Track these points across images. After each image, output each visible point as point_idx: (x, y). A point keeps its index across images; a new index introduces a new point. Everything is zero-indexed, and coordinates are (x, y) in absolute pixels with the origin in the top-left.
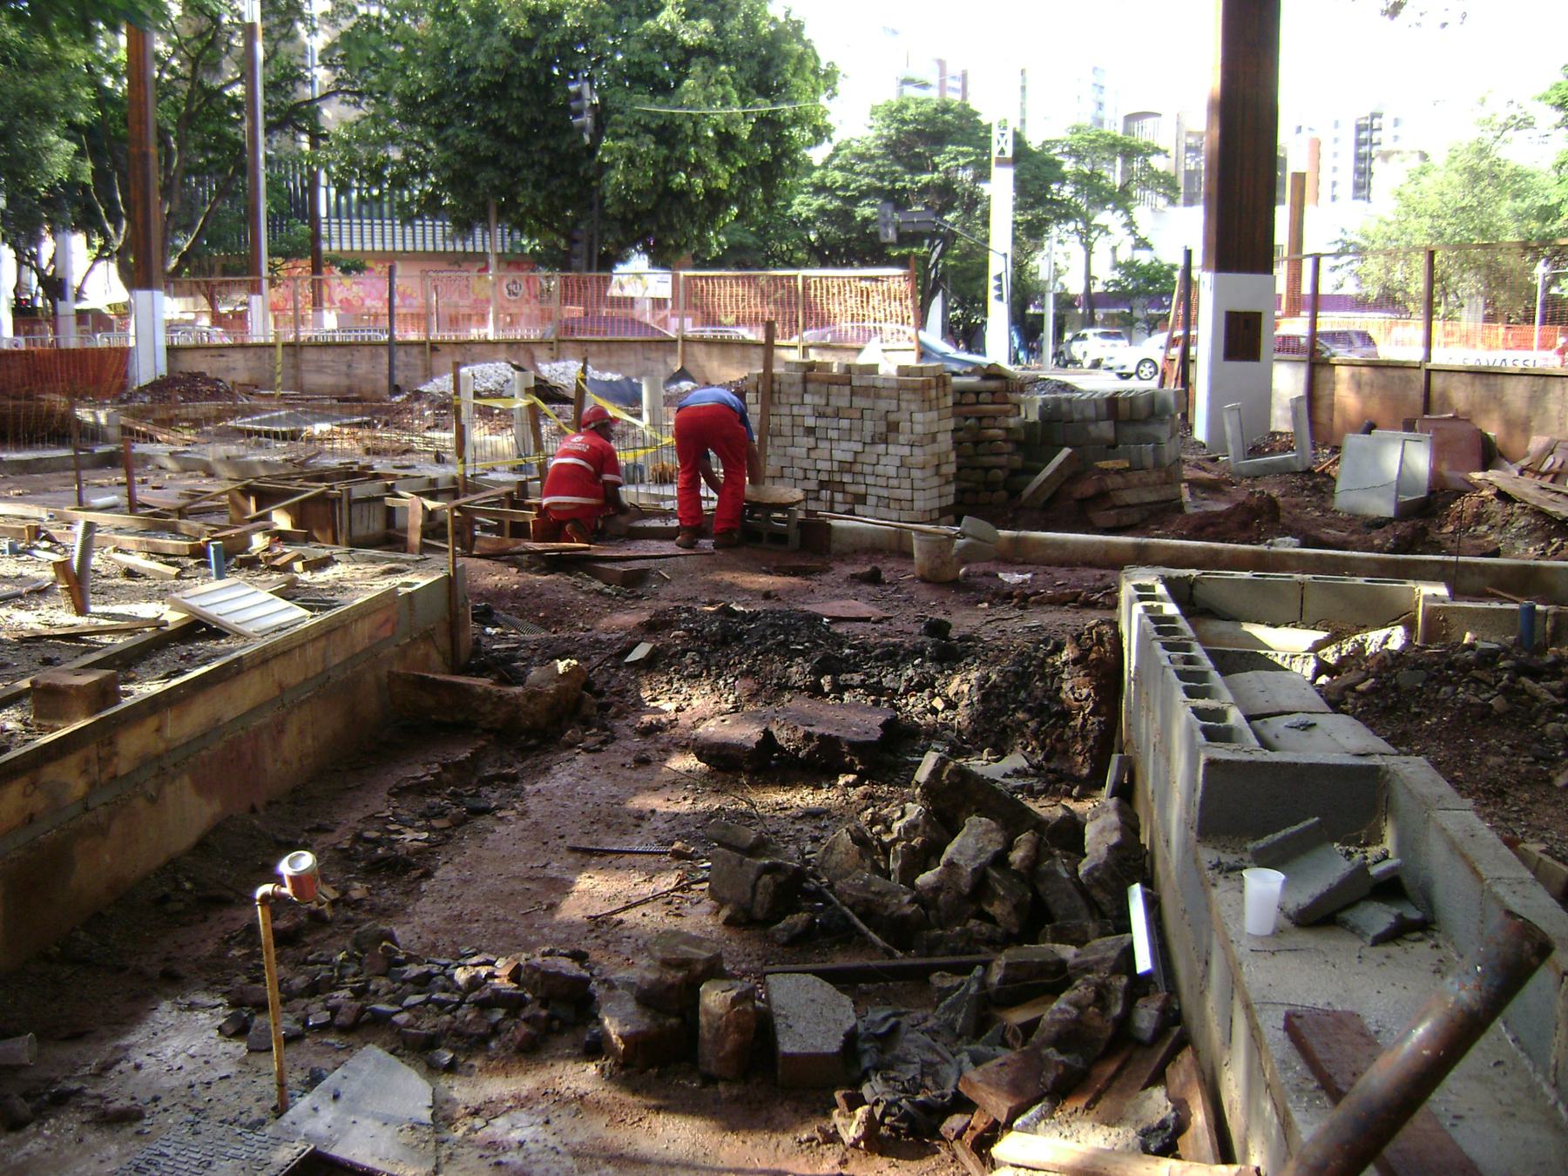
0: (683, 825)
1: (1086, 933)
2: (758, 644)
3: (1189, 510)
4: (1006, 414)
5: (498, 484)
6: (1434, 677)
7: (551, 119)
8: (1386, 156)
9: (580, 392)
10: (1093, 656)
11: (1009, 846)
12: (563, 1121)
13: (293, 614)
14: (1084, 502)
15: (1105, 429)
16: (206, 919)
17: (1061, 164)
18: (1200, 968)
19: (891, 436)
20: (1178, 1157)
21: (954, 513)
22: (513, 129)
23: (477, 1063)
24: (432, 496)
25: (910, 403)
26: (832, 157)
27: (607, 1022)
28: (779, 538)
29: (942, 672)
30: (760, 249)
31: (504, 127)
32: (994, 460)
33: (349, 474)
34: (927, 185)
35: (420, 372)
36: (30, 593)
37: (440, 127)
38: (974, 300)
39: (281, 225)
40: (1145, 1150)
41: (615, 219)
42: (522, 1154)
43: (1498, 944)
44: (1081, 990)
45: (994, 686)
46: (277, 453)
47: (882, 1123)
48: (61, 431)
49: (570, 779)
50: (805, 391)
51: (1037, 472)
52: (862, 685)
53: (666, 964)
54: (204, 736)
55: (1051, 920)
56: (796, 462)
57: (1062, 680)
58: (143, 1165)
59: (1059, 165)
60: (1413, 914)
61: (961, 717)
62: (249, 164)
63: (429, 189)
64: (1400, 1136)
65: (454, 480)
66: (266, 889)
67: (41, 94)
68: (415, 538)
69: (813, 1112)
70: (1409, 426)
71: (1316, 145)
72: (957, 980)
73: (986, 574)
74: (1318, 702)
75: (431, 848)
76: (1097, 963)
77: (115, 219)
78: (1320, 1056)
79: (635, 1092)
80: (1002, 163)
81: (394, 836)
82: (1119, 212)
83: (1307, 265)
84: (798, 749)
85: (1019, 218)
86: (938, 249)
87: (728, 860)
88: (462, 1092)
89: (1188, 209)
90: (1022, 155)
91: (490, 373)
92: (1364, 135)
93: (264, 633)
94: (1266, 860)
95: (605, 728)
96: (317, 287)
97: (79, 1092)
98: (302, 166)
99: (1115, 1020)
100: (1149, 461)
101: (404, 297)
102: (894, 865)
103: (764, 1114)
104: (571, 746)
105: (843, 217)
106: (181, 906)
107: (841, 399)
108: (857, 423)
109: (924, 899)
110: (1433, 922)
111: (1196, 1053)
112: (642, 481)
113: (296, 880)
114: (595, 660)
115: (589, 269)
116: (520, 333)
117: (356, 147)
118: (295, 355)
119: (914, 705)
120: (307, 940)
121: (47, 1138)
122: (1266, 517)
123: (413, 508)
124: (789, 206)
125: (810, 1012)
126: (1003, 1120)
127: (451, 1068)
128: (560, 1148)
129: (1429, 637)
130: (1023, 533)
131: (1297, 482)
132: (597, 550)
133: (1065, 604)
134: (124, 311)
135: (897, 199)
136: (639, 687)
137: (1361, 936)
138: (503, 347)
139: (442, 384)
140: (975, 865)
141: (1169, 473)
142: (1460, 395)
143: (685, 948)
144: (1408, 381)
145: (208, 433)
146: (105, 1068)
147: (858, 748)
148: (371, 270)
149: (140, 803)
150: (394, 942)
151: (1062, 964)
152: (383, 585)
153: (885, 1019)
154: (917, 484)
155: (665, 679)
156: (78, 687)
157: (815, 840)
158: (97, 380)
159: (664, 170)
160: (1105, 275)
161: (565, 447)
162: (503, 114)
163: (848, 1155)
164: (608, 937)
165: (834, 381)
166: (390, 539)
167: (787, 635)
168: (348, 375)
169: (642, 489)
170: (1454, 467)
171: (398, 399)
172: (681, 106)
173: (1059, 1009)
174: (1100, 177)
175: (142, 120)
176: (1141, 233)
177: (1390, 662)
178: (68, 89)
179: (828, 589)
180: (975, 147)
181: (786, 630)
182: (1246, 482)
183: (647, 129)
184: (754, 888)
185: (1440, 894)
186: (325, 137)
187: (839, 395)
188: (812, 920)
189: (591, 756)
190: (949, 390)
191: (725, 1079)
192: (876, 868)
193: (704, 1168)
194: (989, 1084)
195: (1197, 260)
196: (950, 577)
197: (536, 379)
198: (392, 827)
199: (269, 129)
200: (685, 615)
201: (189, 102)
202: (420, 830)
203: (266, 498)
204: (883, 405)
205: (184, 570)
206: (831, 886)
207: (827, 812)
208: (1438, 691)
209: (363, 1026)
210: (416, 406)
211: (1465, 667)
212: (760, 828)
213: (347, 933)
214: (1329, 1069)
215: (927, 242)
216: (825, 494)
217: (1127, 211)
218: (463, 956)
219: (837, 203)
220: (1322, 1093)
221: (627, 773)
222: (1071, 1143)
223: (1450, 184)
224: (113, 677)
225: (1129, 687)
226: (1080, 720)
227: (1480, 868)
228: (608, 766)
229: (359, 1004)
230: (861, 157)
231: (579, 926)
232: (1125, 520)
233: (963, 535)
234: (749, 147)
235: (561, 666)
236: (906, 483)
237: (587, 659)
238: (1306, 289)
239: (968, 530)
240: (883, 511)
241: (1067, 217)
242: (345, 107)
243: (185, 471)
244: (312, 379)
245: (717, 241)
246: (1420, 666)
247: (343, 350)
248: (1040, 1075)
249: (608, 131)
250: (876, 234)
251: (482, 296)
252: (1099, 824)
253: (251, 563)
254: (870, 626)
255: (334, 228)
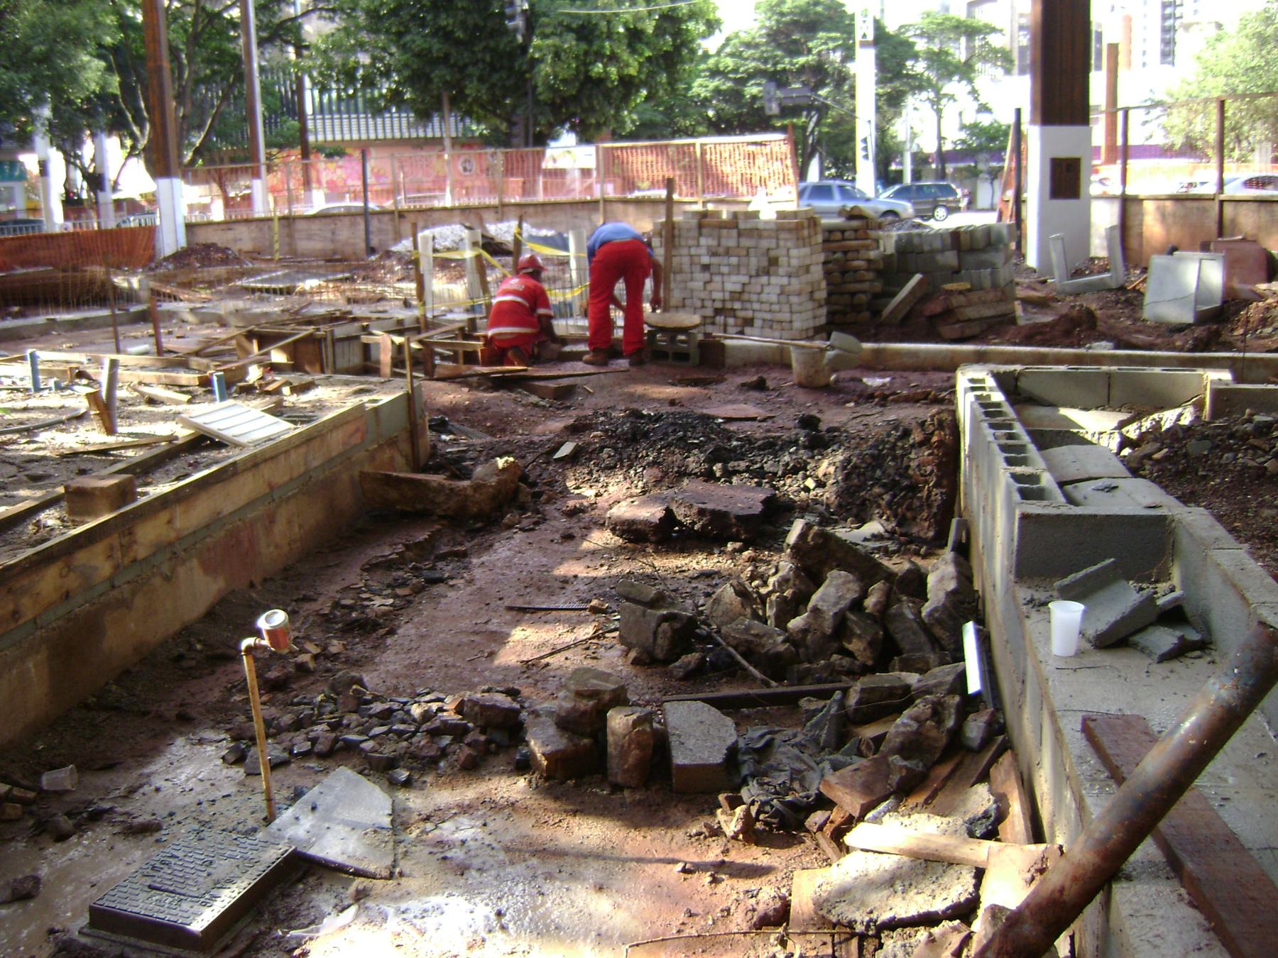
0: (600, 586)
1: (927, 663)
2: (662, 439)
3: (1021, 322)
4: (867, 248)
5: (453, 321)
6: (1218, 446)
7: (490, 24)
8: (1187, 27)
9: (518, 243)
10: (935, 439)
11: (864, 595)
12: (497, 823)
13: (280, 428)
14: (932, 318)
15: (950, 258)
16: (213, 673)
17: (913, 44)
18: (1019, 685)
19: (772, 269)
20: (998, 840)
21: (823, 331)
22: (460, 34)
23: (429, 779)
24: (400, 332)
25: (787, 241)
26: (724, 46)
27: (532, 743)
28: (682, 357)
29: (813, 457)
30: (669, 126)
31: (452, 32)
32: (858, 286)
33: (332, 319)
34: (803, 66)
35: (391, 236)
36: (69, 419)
37: (400, 35)
38: (846, 160)
39: (276, 123)
40: (971, 834)
41: (546, 104)
42: (464, 850)
43: (1252, 650)
44: (920, 707)
45: (855, 467)
46: (275, 306)
47: (757, 819)
48: (103, 295)
49: (509, 553)
50: (700, 234)
51: (894, 295)
52: (747, 470)
53: (579, 694)
54: (208, 526)
55: (899, 653)
56: (695, 294)
57: (910, 460)
58: (158, 865)
59: (912, 45)
60: (1193, 636)
61: (828, 494)
62: (246, 72)
63: (394, 86)
64: (1173, 811)
65: (417, 320)
66: (248, 642)
67: (74, 22)
68: (386, 368)
69: (702, 812)
70: (1205, 247)
71: (1128, 20)
72: (822, 703)
73: (853, 379)
74: (1121, 469)
75: (395, 611)
76: (936, 686)
77: (140, 122)
78: (1109, 752)
79: (556, 799)
80: (864, 44)
81: (366, 603)
82: (964, 82)
83: (1120, 115)
84: (694, 523)
85: (881, 91)
86: (814, 119)
87: (634, 612)
88: (415, 801)
90: (881, 38)
91: (450, 233)
92: (1168, 11)
93: (256, 443)
94: (1069, 594)
95: (538, 513)
96: (306, 169)
97: (111, 810)
98: (290, 74)
99: (949, 731)
100: (987, 283)
101: (378, 176)
102: (770, 612)
103: (662, 814)
104: (510, 527)
105: (734, 95)
106: (193, 663)
107: (730, 240)
108: (744, 260)
109: (794, 640)
110: (1211, 643)
111: (1015, 757)
112: (572, 316)
113: (273, 633)
114: (530, 458)
115: (527, 145)
116: (474, 201)
117: (331, 54)
118: (289, 226)
119: (791, 487)
120: (294, 686)
121: (85, 846)
122: (1084, 326)
123: (384, 343)
124: (689, 88)
125: (699, 733)
126: (856, 814)
127: (407, 784)
128: (495, 845)
129: (1215, 414)
130: (883, 345)
131: (1112, 297)
132: (533, 371)
133: (917, 401)
134: (153, 199)
135: (778, 79)
136: (565, 478)
137: (1150, 655)
138: (457, 213)
139: (405, 245)
140: (836, 610)
141: (1003, 292)
143: (595, 682)
144: (1205, 210)
145: (220, 292)
146: (132, 791)
147: (744, 520)
148: (350, 155)
149: (157, 581)
150: (363, 685)
151: (907, 688)
152: (352, 402)
153: (762, 736)
154: (795, 308)
155: (586, 471)
156: (102, 489)
157: (708, 595)
158: (131, 253)
159: (585, 61)
160: (954, 137)
161: (505, 286)
162: (451, 21)
163: (730, 845)
164: (537, 677)
165: (723, 226)
166: (367, 367)
167: (685, 432)
168: (333, 241)
169: (571, 322)
170: (1244, 281)
171: (373, 258)
172: (596, 8)
173: (903, 722)
174: (947, 54)
175: (156, 41)
176: (983, 100)
177: (1177, 433)
178: (95, 18)
179: (723, 396)
180: (843, 33)
181: (684, 427)
182: (1068, 299)
183: (569, 29)
184: (655, 633)
185: (1216, 619)
186: (307, 47)
187: (729, 237)
188: (703, 658)
189: (526, 534)
190: (819, 229)
191: (629, 787)
192: (755, 616)
193: (611, 859)
194: (845, 785)
195: (1026, 116)
196: (822, 382)
197: (483, 236)
198: (364, 596)
199: (262, 43)
200: (602, 419)
201: (195, 23)
202: (387, 596)
203: (265, 340)
204: (765, 244)
205: (194, 397)
206: (718, 632)
207: (717, 573)
208: (1221, 457)
209: (337, 752)
210: (388, 263)
211: (1244, 437)
212: (662, 587)
213: (326, 680)
214: (1117, 761)
215: (805, 113)
216: (720, 319)
217: (970, 81)
218: (419, 695)
219: (729, 84)
220: (1111, 782)
221: (556, 547)
222: (910, 830)
223: (1241, 47)
224: (130, 481)
225: (964, 463)
226: (925, 492)
227: (1248, 595)
228: (539, 542)
229: (334, 735)
230: (748, 45)
231: (514, 668)
232: (968, 332)
233: (832, 347)
234: (654, 40)
235: (501, 462)
236: (786, 308)
237: (523, 457)
238: (1120, 142)
239: (836, 344)
240: (767, 331)
241: (921, 88)
242: (322, 23)
243: (202, 322)
244: (303, 245)
245: (630, 119)
246: (1206, 437)
247: (328, 221)
248: (887, 777)
249: (537, 32)
250: (762, 109)
251: (441, 174)
252: (940, 575)
253: (248, 391)
254: (756, 424)
255: (319, 123)
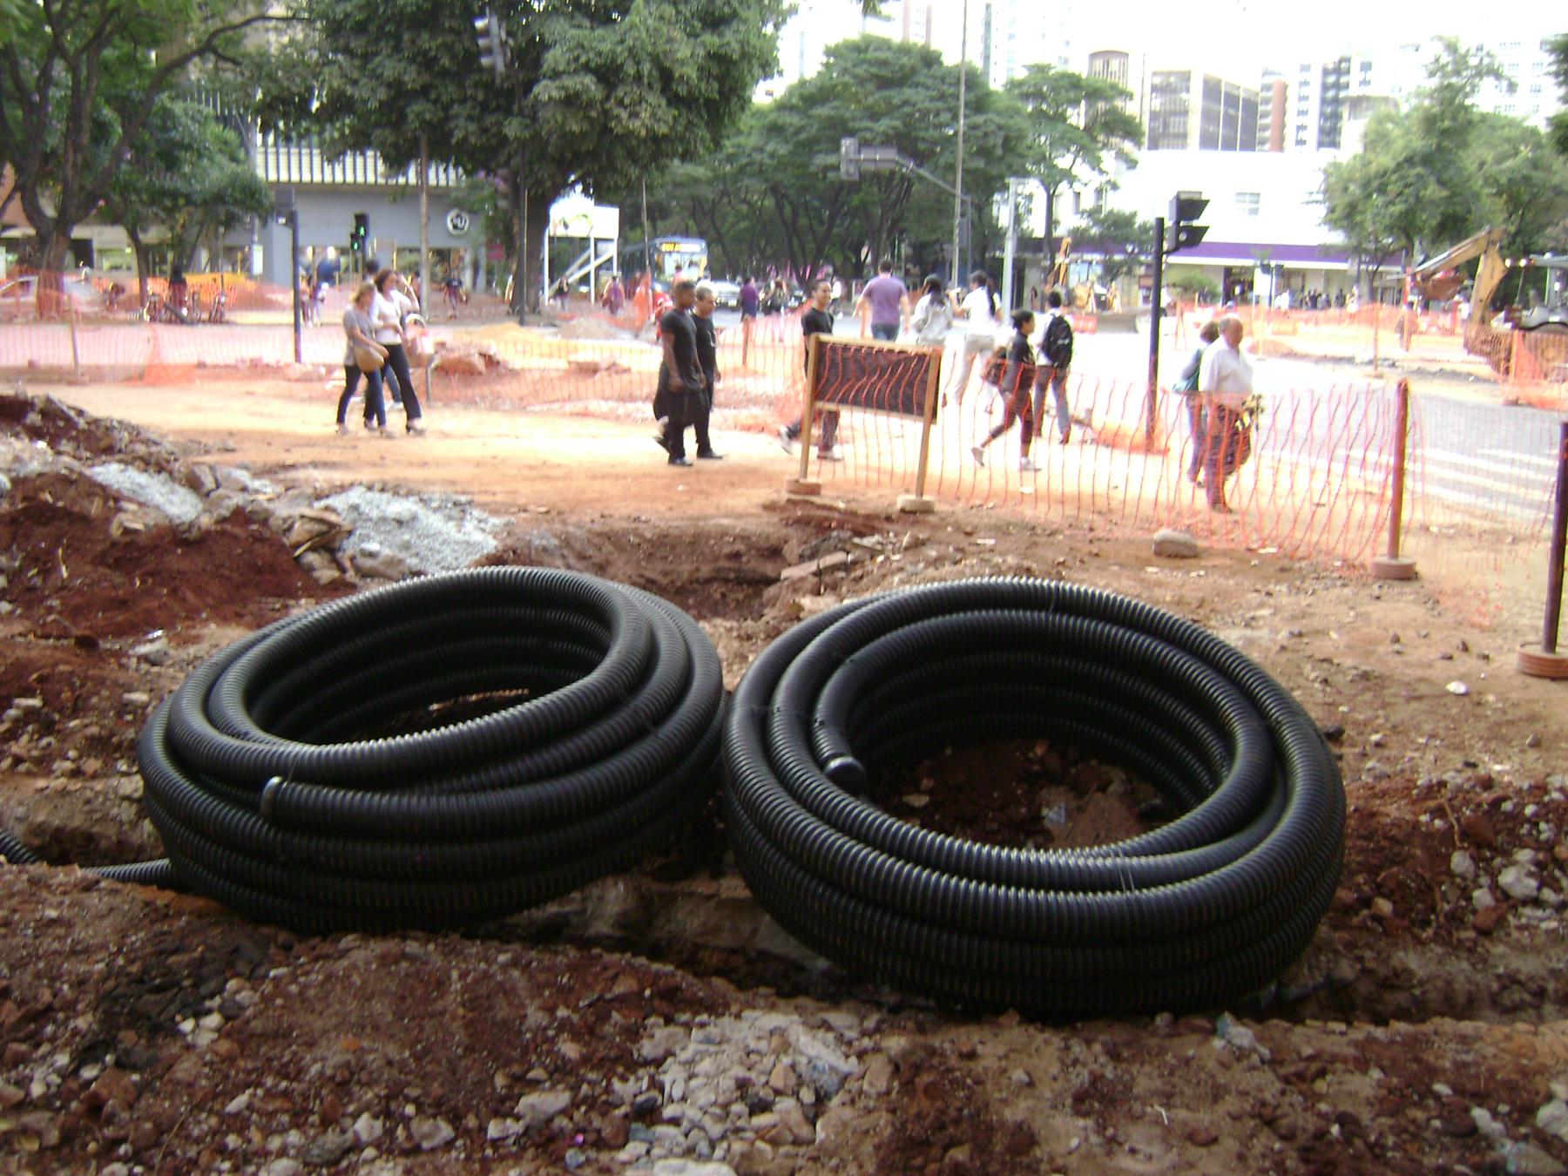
22: (446, 61)
31: (435, 59)
89: (1154, 152)
142: (1385, 160)
